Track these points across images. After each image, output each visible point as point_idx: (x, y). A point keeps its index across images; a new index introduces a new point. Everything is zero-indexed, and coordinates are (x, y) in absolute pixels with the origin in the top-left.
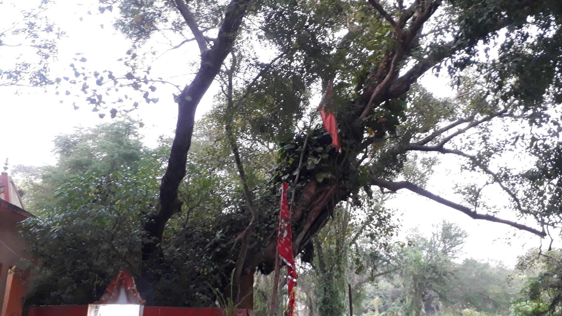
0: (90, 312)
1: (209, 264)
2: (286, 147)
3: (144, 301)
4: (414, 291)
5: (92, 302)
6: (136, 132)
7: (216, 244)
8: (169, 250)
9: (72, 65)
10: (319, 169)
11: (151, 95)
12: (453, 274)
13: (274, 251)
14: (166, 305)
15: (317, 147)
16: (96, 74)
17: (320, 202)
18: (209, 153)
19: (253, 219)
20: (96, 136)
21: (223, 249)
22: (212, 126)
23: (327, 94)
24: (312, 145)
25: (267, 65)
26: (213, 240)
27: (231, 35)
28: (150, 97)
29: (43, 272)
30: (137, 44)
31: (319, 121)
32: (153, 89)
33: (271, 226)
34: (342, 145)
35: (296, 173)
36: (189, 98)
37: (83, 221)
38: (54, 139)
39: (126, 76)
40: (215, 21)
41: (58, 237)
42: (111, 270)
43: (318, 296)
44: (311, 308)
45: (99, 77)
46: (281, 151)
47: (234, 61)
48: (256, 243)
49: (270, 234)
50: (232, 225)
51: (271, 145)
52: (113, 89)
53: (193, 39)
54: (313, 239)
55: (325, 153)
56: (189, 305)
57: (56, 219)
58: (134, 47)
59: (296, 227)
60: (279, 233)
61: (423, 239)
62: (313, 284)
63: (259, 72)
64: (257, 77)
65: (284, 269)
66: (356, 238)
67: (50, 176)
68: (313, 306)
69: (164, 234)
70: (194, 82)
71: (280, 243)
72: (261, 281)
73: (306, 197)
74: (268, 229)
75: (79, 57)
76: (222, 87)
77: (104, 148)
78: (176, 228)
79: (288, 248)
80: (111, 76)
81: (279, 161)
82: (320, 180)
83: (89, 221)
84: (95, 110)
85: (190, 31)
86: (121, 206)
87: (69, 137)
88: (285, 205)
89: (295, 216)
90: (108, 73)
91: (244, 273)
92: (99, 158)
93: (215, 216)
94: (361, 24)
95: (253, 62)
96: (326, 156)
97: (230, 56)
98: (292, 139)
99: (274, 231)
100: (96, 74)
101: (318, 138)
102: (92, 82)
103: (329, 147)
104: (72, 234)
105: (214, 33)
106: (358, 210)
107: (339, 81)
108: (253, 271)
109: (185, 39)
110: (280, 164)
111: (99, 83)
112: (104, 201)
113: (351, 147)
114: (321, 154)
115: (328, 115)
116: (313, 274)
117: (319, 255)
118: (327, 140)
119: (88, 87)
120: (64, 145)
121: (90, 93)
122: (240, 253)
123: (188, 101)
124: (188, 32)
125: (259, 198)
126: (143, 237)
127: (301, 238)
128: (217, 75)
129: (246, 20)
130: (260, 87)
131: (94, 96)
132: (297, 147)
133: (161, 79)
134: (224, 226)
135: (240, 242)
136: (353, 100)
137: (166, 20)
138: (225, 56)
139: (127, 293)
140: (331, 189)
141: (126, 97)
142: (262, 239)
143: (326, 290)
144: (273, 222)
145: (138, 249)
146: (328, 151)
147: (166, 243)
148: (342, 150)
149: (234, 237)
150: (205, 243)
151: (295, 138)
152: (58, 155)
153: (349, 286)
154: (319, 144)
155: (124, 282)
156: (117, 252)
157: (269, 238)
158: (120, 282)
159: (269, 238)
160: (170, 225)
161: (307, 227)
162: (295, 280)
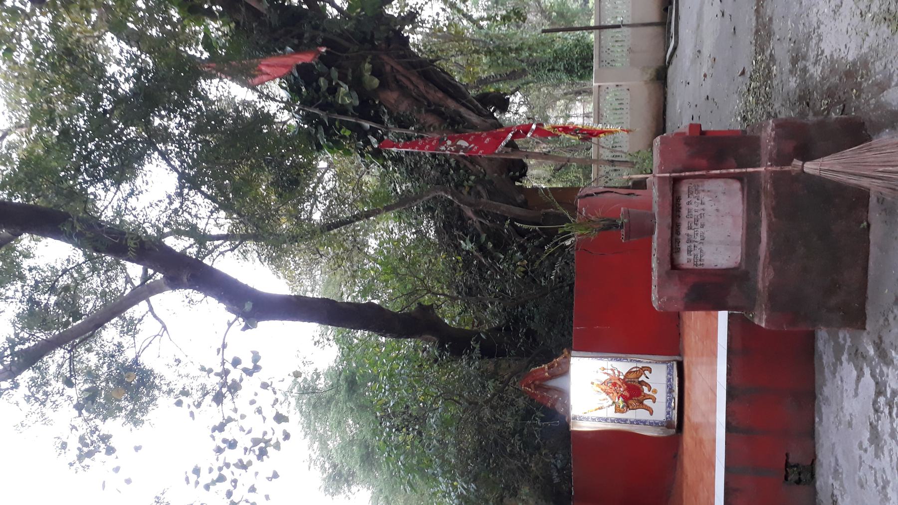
0: (580, 427)
1: (511, 259)
2: (323, 141)
3: (565, 351)
5: (567, 426)
6: (312, 377)
7: (481, 248)
8: (492, 318)
9: (207, 487)
10: (357, 85)
11: (248, 363)
13: (491, 160)
14: (571, 319)
15: (318, 88)
16: (219, 450)
17: (412, 82)
18: (339, 266)
19: (443, 194)
20: (321, 436)
21: (488, 238)
22: (295, 261)
23: (222, 72)
24: (316, 96)
25: (180, 179)
26: (475, 253)
27: (131, 243)
28: (250, 366)
29: (524, 498)
30: (165, 388)
31: (276, 88)
32: (236, 362)
33: (453, 165)
34: (312, 44)
35: (367, 125)
36: (248, 306)
37: (451, 449)
38: (329, 496)
39: (218, 405)
40: (110, 267)
41: (474, 482)
42: (521, 402)
43: (560, 80)
44: (579, 93)
45: (223, 446)
46: (331, 149)
47: (177, 233)
48: (480, 188)
49: (465, 166)
50: (452, 225)
51: (323, 164)
52: (242, 423)
53: (148, 302)
54: (472, 92)
55: (329, 74)
56: (571, 286)
57: (447, 487)
58: (170, 391)
59: (455, 125)
60: (461, 153)
62: (544, 89)
63: (192, 193)
64: (203, 193)
65: (519, 142)
66: (470, 18)
67: (386, 497)
68: (576, 89)
69: (467, 328)
70: (221, 299)
71: (477, 152)
72: (538, 176)
73: (404, 107)
74: (457, 169)
75: (193, 478)
76: (222, 253)
77: (339, 423)
78: (458, 310)
79: (485, 138)
80: (221, 428)
81: (347, 153)
82: (376, 82)
83: (449, 439)
84: (277, 446)
85: (135, 307)
86: (425, 394)
87: (325, 475)
88: (418, 145)
89: (437, 125)
90: (216, 433)
91: (524, 205)
92: (356, 429)
93: (440, 253)
94: (93, 10)
95: (176, 204)
96: (334, 73)
97: (170, 241)
98: (308, 132)
99: (460, 159)
100: (219, 450)
101: (304, 87)
102: (233, 456)
103: (319, 67)
104: (469, 461)
105: (135, 270)
106: (424, 15)
107: (200, 48)
108: (522, 189)
109: (150, 313)
110: (353, 150)
111: (232, 445)
112: (421, 419)
113: (316, 28)
114: (330, 81)
115: (261, 70)
116: (528, 90)
117: (498, 81)
118: (305, 71)
119: (241, 461)
120: (338, 481)
121: (252, 457)
122: (495, 211)
123: (252, 307)
124: (138, 310)
125: (409, 184)
126: (471, 358)
127: (472, 114)
128: (204, 261)
129: (108, 215)
130: (221, 189)
131: (254, 451)
132: (321, 122)
133: (219, 350)
134: (453, 238)
135: (477, 213)
136: (233, 25)
137: (120, 345)
138: (170, 251)
139: (553, 376)
140: (390, 64)
141: (253, 402)
142: (473, 178)
143: (553, 70)
144: (447, 161)
145: (490, 365)
146: (325, 69)
147: (480, 323)
148: (322, 45)
149: (470, 222)
150: (480, 265)
151: (306, 126)
152: (354, 488)
153: (544, 31)
154: (314, 84)
155: (537, 382)
156: (493, 395)
157: (471, 167)
158: (537, 387)
159: (471, 167)
160: (453, 318)
161: (452, 105)
162: (534, 127)
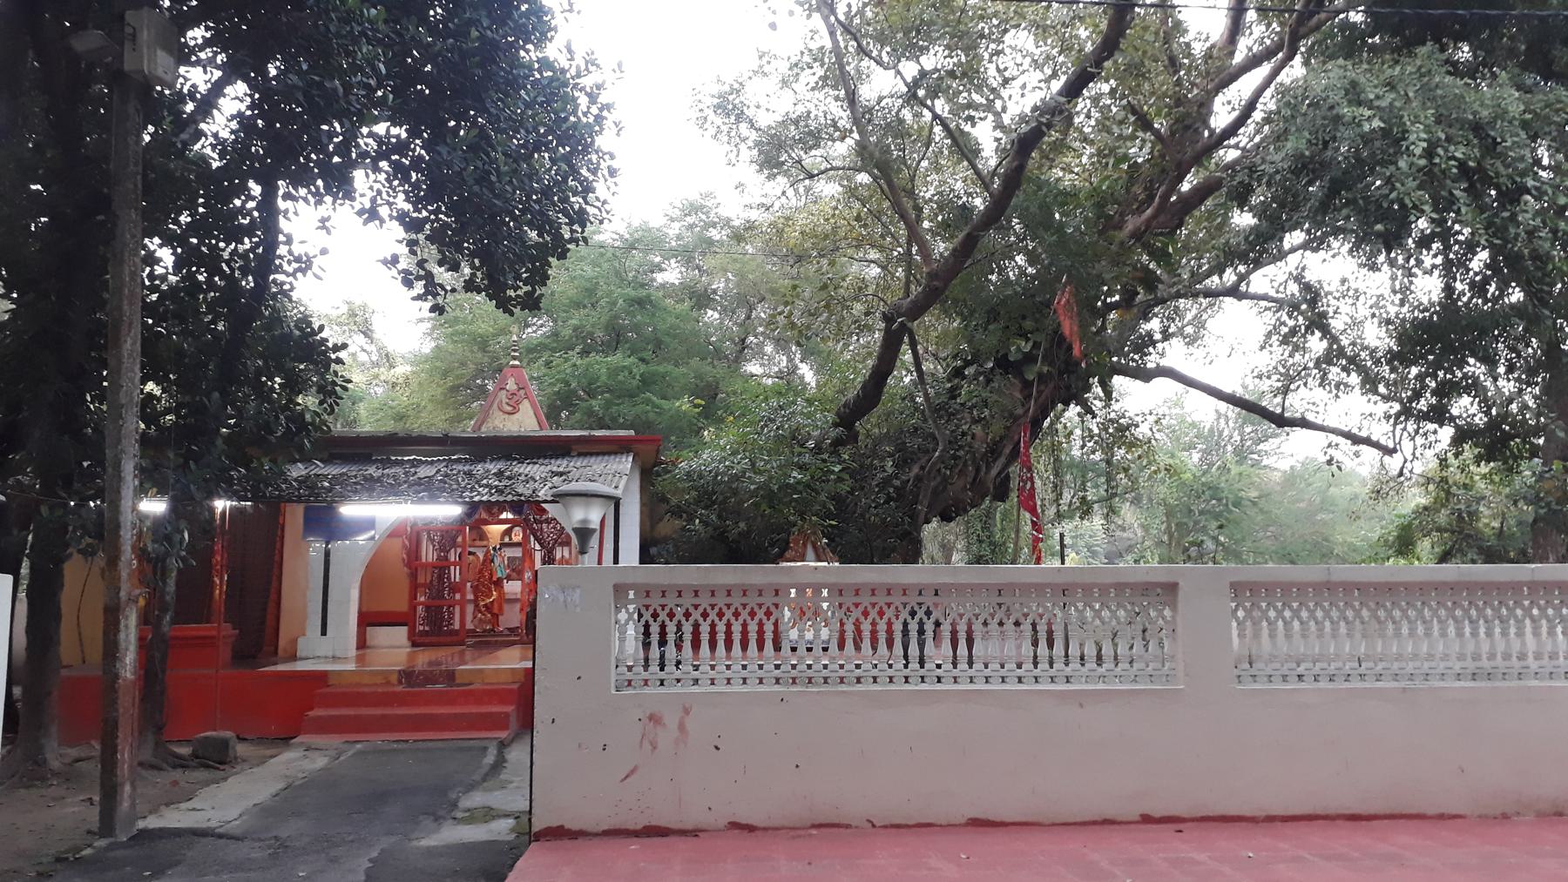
4: (1165, 538)
12: (1254, 504)
61: (1193, 425)
135: (918, 479)
